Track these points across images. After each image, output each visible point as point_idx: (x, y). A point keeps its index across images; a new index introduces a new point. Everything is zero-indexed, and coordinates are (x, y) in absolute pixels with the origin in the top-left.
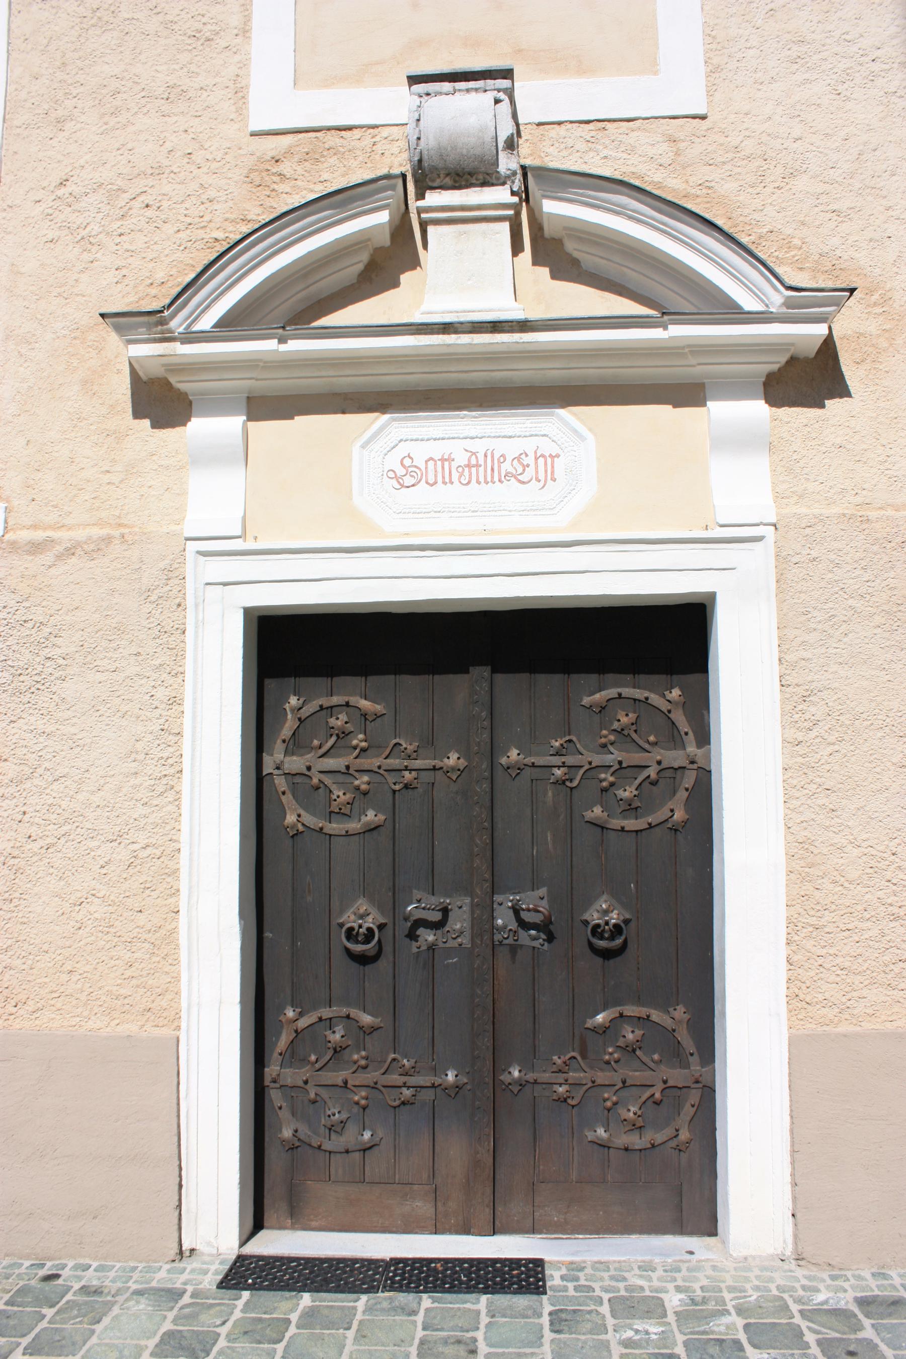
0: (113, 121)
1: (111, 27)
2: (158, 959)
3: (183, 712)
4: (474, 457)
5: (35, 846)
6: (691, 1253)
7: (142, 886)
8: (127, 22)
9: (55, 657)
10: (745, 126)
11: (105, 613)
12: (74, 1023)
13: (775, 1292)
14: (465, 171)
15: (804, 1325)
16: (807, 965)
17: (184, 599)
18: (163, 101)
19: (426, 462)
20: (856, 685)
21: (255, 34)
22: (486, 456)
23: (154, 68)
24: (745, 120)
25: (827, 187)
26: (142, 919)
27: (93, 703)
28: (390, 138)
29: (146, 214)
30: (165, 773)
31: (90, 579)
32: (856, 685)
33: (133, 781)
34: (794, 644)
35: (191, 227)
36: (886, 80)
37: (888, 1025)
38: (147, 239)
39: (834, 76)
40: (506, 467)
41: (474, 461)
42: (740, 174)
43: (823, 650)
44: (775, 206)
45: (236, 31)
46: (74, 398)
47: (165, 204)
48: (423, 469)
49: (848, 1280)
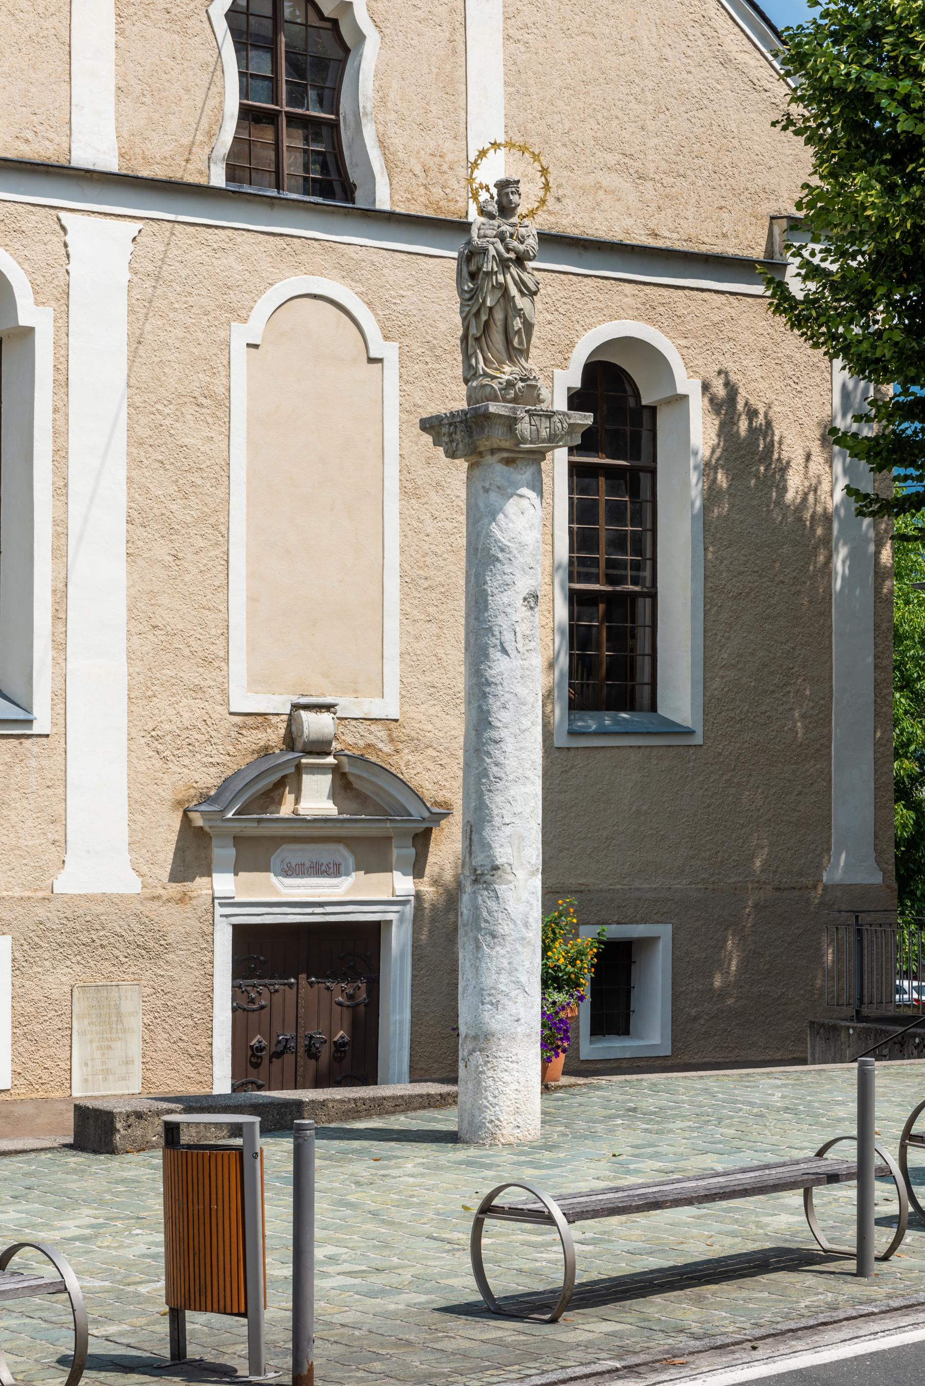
5: (158, 1021)
26: (198, 1048)
40: (323, 868)
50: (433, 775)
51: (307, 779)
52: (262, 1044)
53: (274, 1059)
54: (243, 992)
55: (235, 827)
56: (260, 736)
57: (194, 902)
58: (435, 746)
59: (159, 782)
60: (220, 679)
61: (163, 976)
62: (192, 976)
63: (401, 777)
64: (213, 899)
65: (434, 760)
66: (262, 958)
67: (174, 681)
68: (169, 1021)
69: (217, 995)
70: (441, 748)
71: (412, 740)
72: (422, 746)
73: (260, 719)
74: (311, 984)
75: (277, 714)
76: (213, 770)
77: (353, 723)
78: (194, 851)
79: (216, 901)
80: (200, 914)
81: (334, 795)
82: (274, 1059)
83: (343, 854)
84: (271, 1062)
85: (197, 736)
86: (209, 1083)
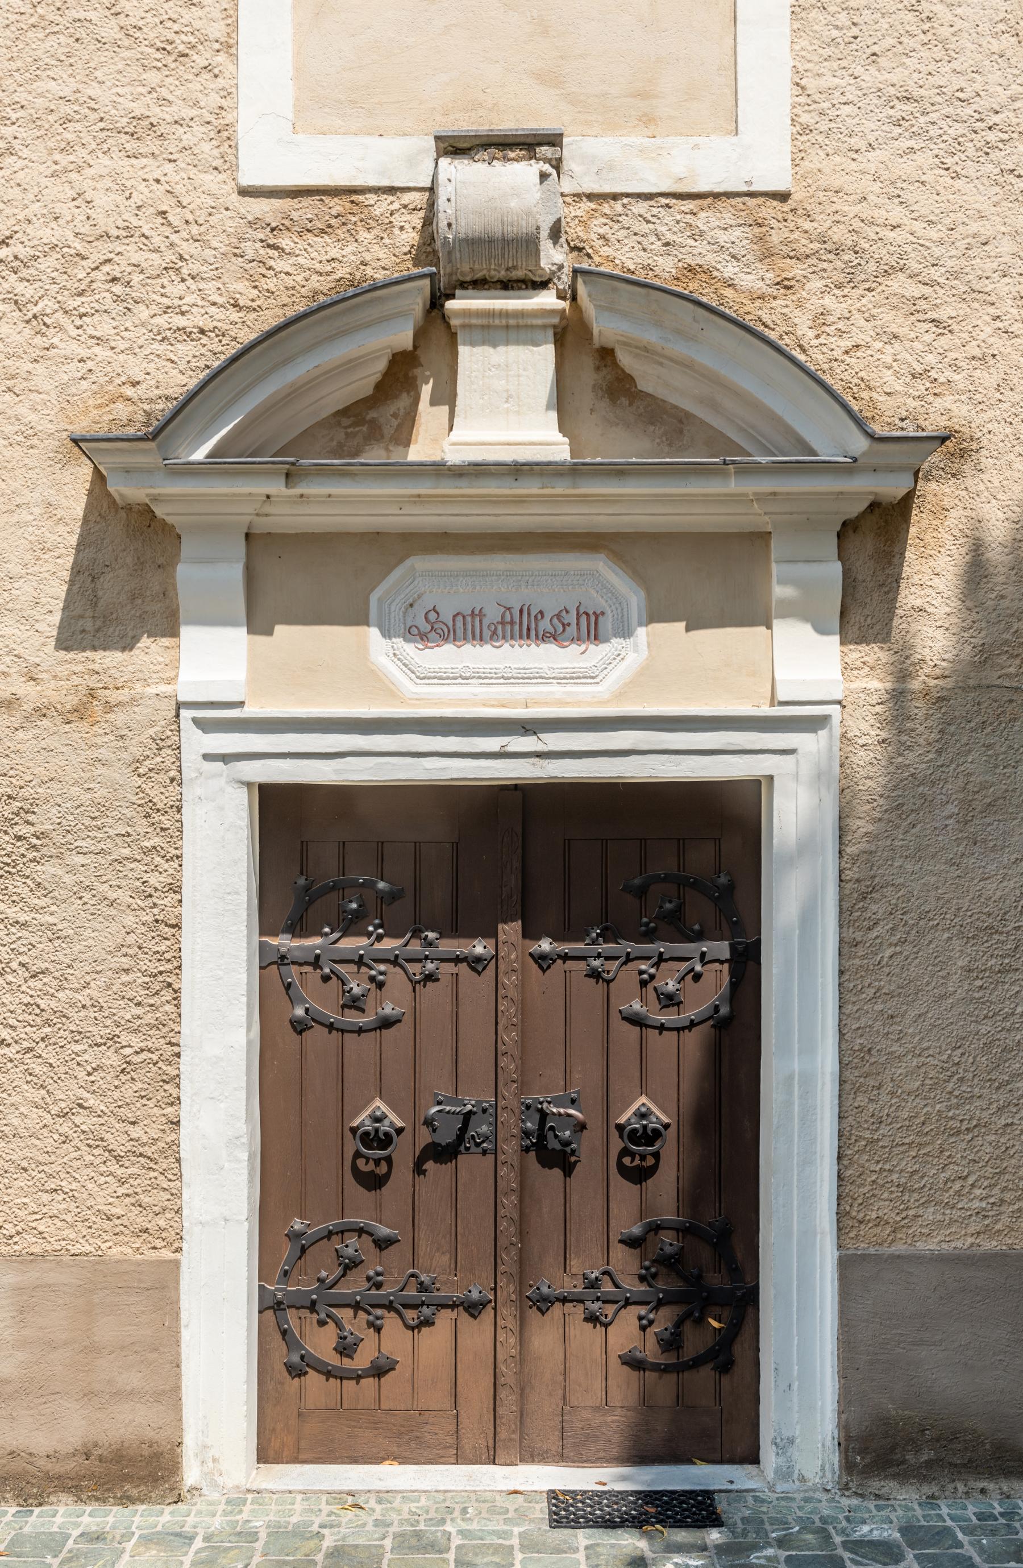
0: (64, 160)
1: (56, 29)
2: (156, 1174)
3: (180, 901)
4: (508, 612)
6: (732, 1482)
7: (137, 1094)
8: (78, 24)
9: (28, 835)
10: (835, 207)
11: (86, 786)
12: (59, 1248)
13: (818, 1523)
14: (503, 262)
15: (847, 1555)
16: (859, 1181)
17: (180, 772)
18: (127, 137)
19: (455, 616)
20: (923, 881)
21: (243, 52)
22: (521, 611)
23: (115, 90)
24: (835, 199)
25: (927, 290)
26: (136, 1132)
27: (75, 889)
28: (410, 207)
29: (113, 289)
30: (162, 969)
31: (67, 745)
32: (923, 881)
33: (125, 978)
34: (856, 835)
35: (169, 311)
36: (1003, 153)
37: (945, 1246)
38: (115, 324)
39: (942, 145)
40: (545, 625)
41: (508, 618)
42: (825, 270)
43: (888, 843)
44: (863, 312)
45: (217, 46)
46: (34, 523)
47: (136, 278)
48: (451, 625)
49: (895, 1510)
50: (911, 351)
51: (473, 360)
52: (385, 1127)
53: (429, 1165)
54: (326, 979)
55: (233, 499)
56: (334, 253)
57: (120, 717)
58: (914, 266)
59: (19, 385)
60: (214, 100)
61: (24, 925)
62: (114, 927)
63: (802, 358)
64: (179, 706)
65: (913, 308)
66: (381, 885)
67: (67, 109)
68: (49, 1054)
69: (192, 981)
70: (936, 274)
71: (837, 251)
72: (872, 266)
73: (337, 205)
74: (542, 960)
75: (391, 190)
76: (185, 350)
77: (641, 207)
78: (125, 575)
79: (184, 713)
80: (137, 752)
81: (563, 402)
82: (429, 1165)
83: (607, 579)
84: (419, 1169)
85: (137, 257)
86: (171, 1235)
